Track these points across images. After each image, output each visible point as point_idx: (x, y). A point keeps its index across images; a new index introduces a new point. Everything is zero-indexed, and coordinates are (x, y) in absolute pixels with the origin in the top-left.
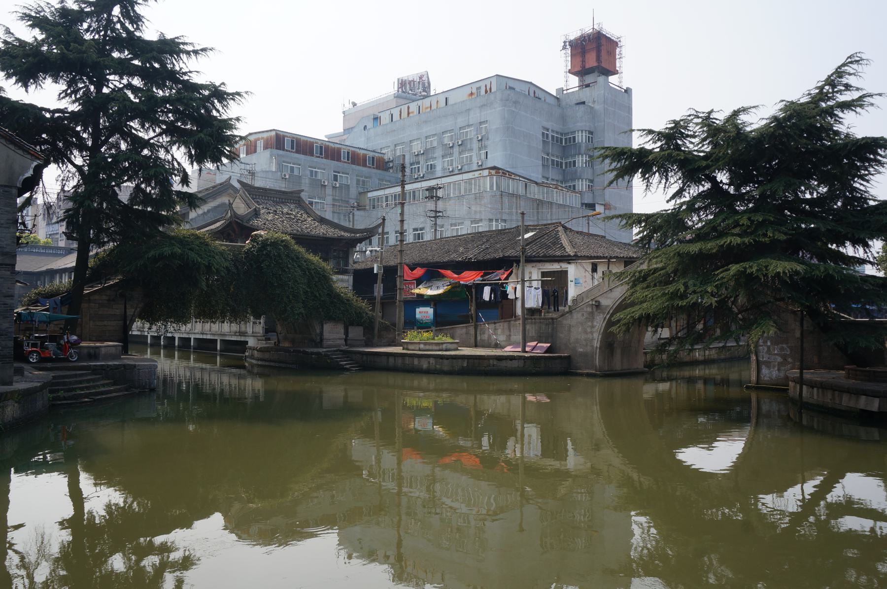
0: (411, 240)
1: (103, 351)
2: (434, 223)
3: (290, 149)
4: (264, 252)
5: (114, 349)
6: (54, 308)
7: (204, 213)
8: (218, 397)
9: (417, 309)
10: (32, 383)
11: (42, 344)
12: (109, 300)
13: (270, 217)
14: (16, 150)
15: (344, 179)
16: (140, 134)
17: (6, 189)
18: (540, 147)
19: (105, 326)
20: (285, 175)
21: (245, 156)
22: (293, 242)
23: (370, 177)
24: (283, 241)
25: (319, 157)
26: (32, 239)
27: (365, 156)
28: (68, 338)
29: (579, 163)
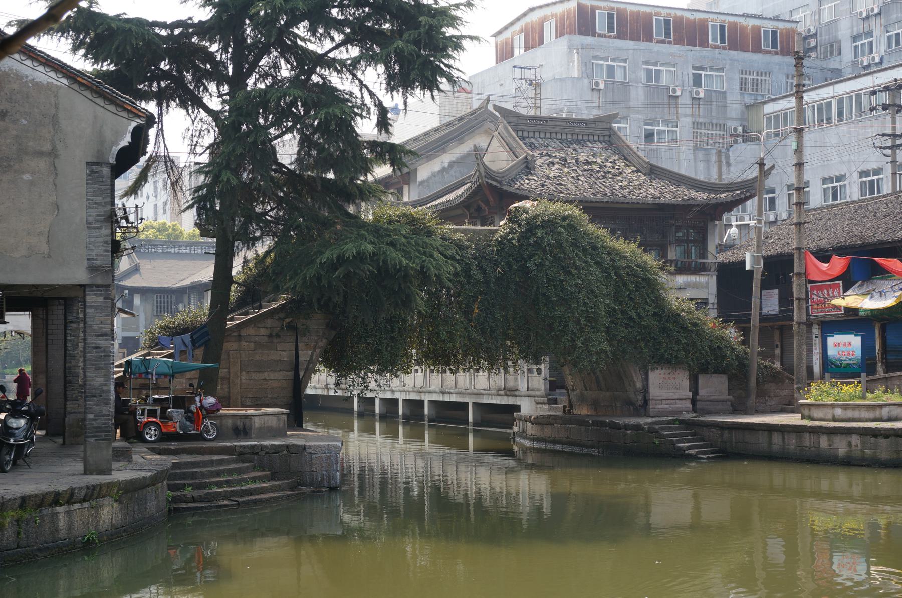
0: (856, 196)
1: (257, 422)
2: (890, 159)
3: (606, 32)
4: (532, 241)
5: (274, 419)
6: (182, 353)
7: (444, 170)
8: (471, 509)
9: (829, 339)
10: (139, 472)
11: (164, 410)
12: (270, 336)
13: (553, 172)
14: (106, 106)
15: (714, 82)
16: (311, 47)
17: (95, 168)
19: (265, 380)
20: (597, 84)
21: (522, 51)
22: (585, 218)
23: (769, 73)
24: (564, 218)
25: (663, 42)
26: (170, 230)
27: (756, 30)
28: (201, 402)
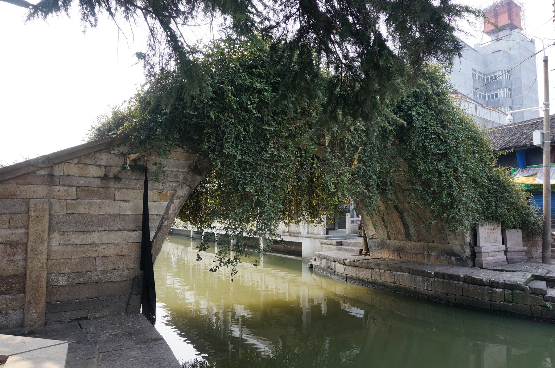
12: (105, 178)
18: (472, 83)
19: (94, 244)
29: (500, 95)
